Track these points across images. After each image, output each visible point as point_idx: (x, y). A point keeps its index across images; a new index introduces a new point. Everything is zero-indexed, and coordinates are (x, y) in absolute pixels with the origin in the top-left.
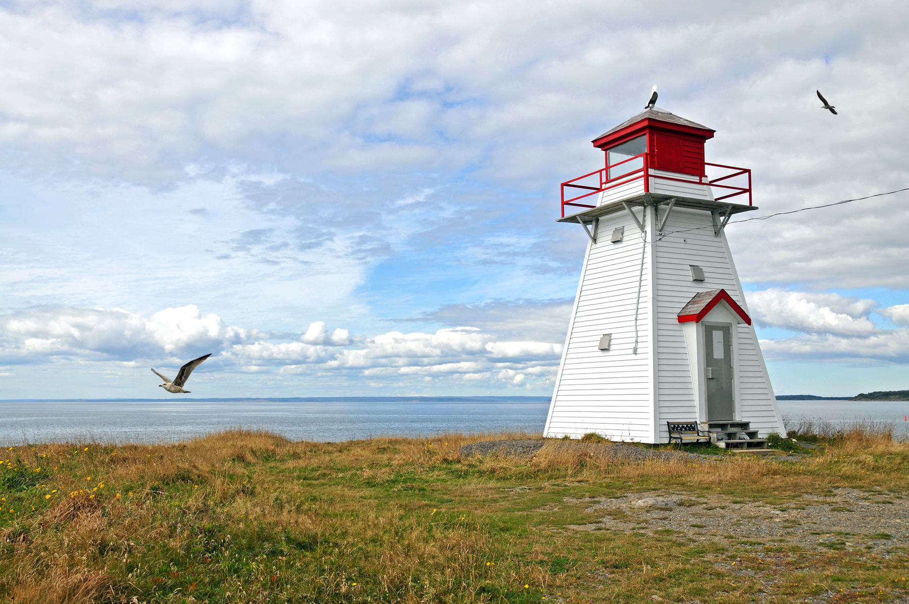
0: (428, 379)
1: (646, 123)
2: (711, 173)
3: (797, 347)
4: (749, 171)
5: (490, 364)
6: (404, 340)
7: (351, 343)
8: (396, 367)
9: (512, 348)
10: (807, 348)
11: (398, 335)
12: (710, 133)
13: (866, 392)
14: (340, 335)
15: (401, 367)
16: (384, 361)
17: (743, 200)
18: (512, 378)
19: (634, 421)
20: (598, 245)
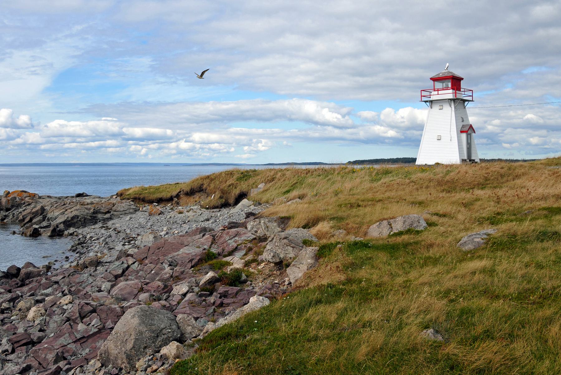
0: (83, 151)
1: (452, 77)
2: (462, 90)
3: (312, 134)
4: (472, 91)
5: (125, 142)
6: (67, 126)
7: (31, 127)
8: (62, 143)
9: (138, 132)
10: (317, 135)
11: (62, 122)
12: (462, 79)
13: (352, 161)
14: (23, 119)
15: (65, 143)
16: (55, 139)
17: (470, 98)
18: (140, 151)
19: (452, 159)
20: (432, 109)
